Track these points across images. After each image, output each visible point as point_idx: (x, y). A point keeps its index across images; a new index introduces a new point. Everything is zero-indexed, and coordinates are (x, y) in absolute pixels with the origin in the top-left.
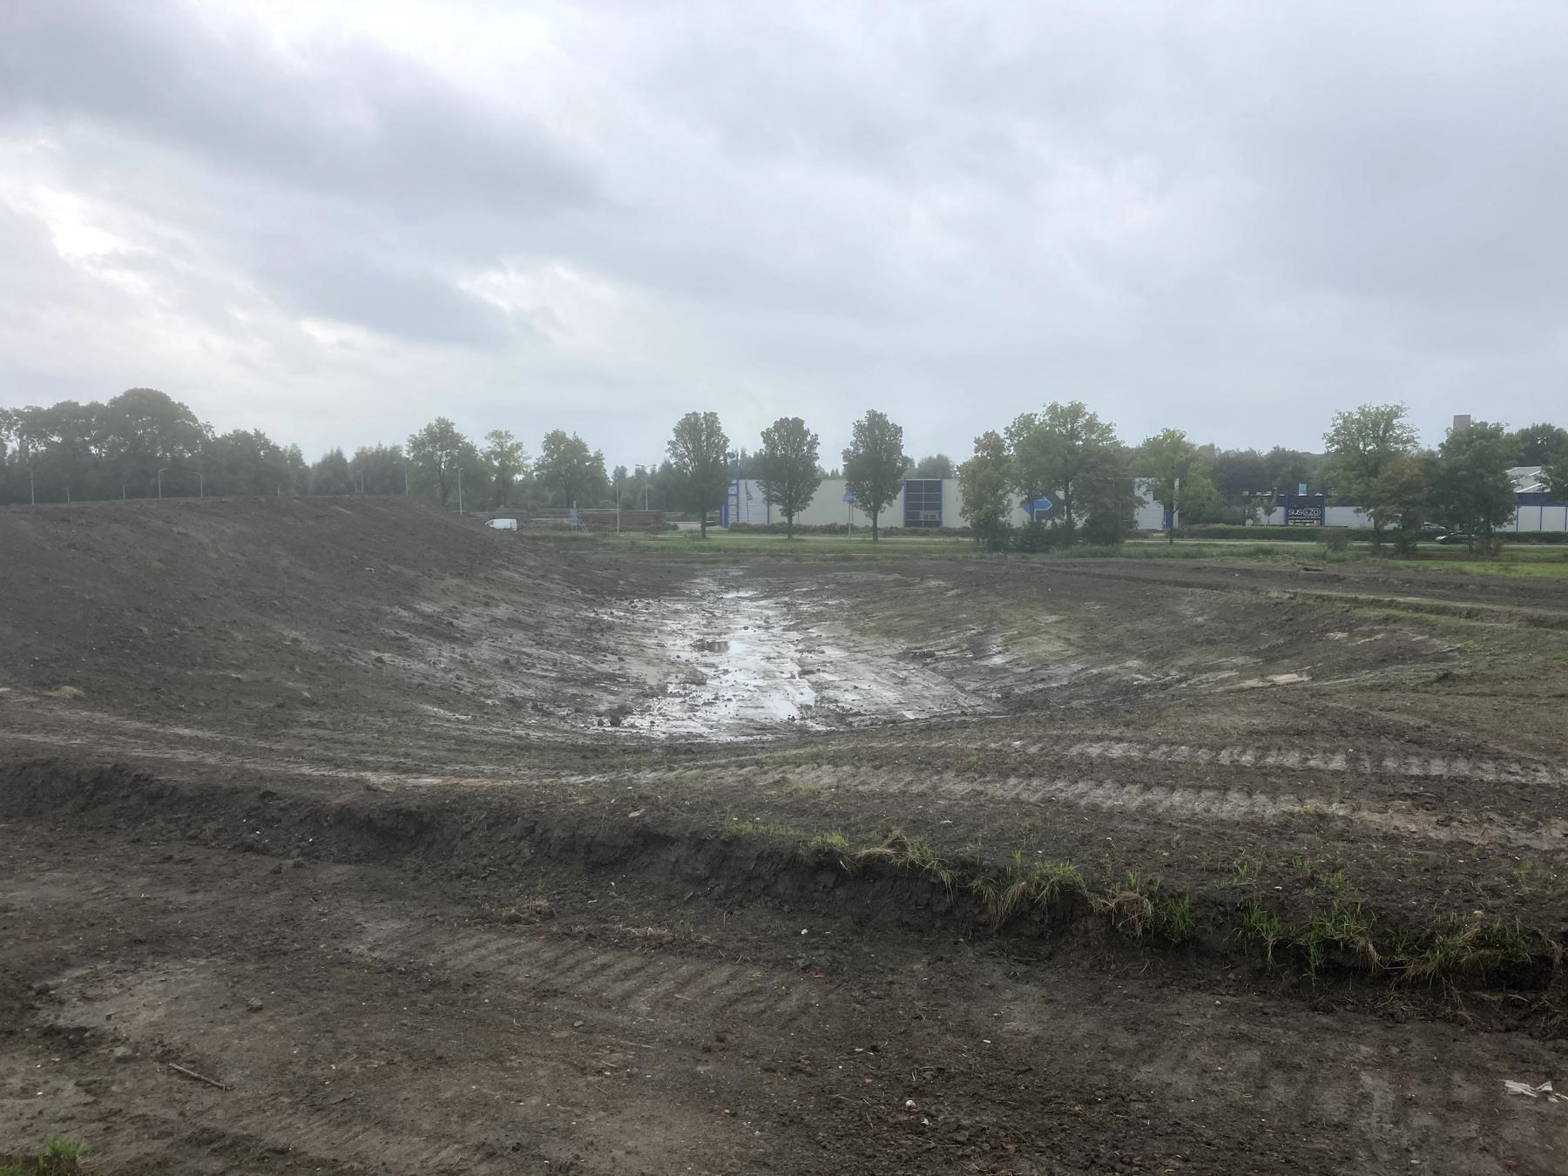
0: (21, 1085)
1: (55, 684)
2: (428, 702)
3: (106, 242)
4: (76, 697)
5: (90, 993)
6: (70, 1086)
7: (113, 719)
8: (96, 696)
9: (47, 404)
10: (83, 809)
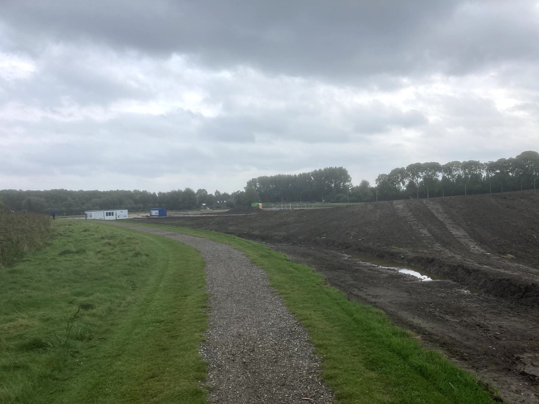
0: (515, 389)
1: (505, 253)
2: (403, 266)
3: (513, 102)
4: (512, 258)
5: (535, 363)
6: (533, 394)
7: (527, 267)
8: (519, 259)
9: (495, 160)
10: (522, 297)
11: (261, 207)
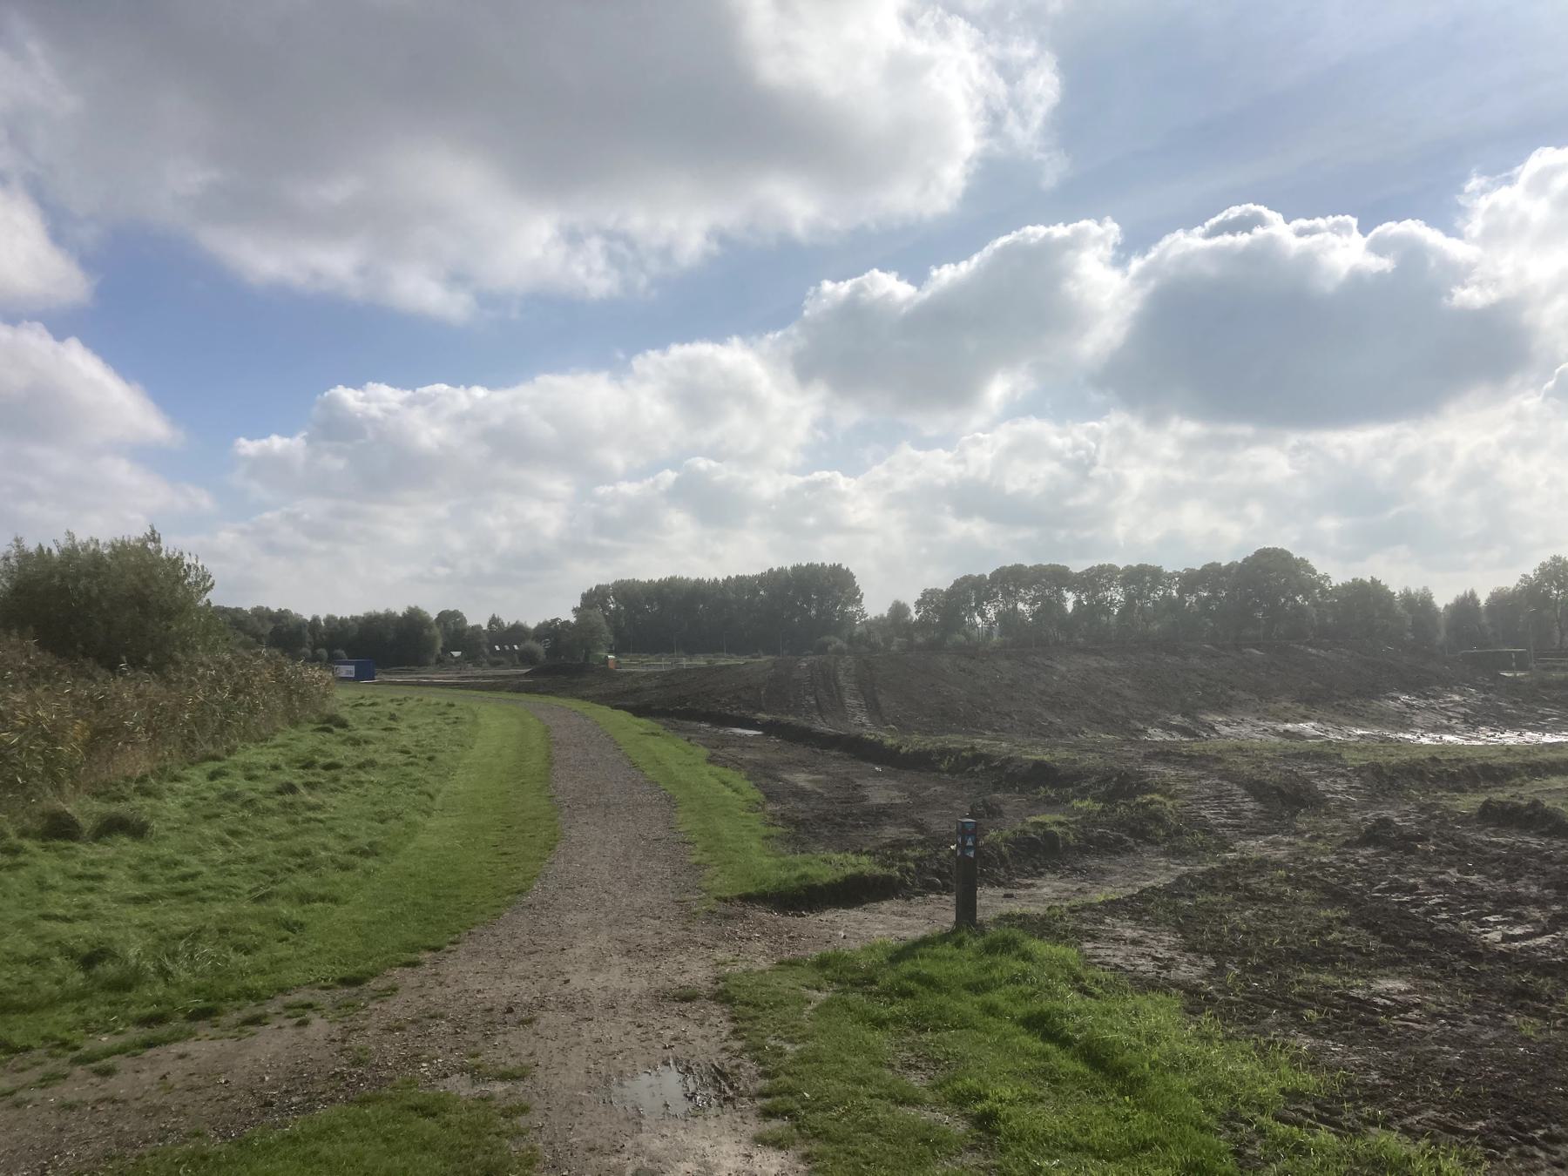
11: (611, 666)
